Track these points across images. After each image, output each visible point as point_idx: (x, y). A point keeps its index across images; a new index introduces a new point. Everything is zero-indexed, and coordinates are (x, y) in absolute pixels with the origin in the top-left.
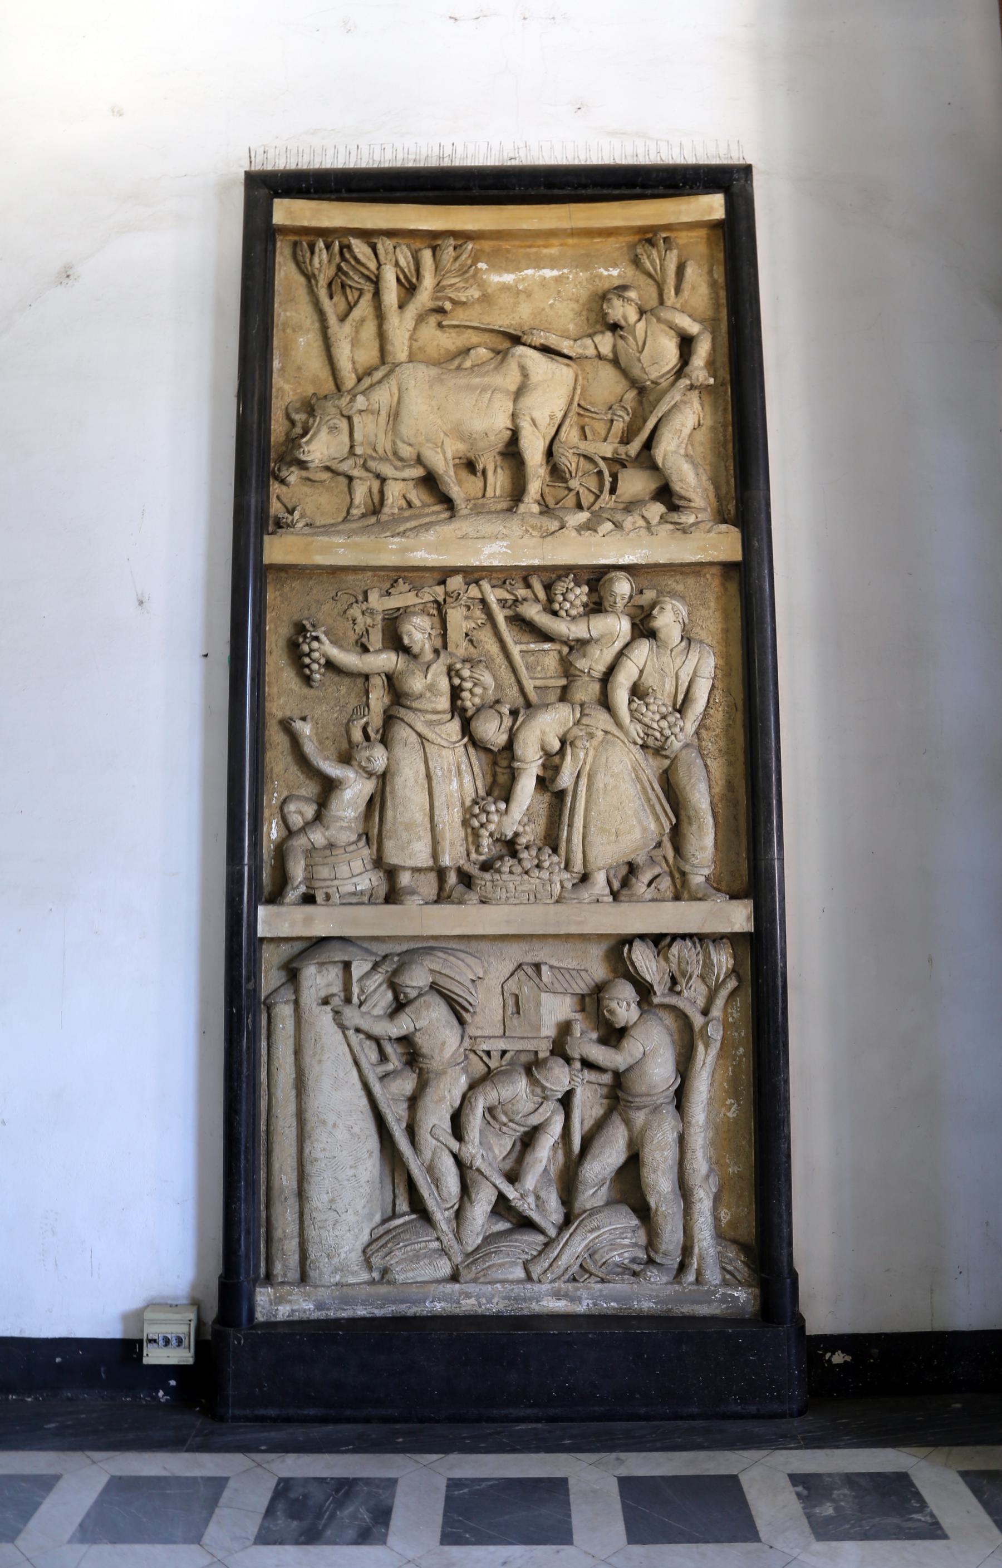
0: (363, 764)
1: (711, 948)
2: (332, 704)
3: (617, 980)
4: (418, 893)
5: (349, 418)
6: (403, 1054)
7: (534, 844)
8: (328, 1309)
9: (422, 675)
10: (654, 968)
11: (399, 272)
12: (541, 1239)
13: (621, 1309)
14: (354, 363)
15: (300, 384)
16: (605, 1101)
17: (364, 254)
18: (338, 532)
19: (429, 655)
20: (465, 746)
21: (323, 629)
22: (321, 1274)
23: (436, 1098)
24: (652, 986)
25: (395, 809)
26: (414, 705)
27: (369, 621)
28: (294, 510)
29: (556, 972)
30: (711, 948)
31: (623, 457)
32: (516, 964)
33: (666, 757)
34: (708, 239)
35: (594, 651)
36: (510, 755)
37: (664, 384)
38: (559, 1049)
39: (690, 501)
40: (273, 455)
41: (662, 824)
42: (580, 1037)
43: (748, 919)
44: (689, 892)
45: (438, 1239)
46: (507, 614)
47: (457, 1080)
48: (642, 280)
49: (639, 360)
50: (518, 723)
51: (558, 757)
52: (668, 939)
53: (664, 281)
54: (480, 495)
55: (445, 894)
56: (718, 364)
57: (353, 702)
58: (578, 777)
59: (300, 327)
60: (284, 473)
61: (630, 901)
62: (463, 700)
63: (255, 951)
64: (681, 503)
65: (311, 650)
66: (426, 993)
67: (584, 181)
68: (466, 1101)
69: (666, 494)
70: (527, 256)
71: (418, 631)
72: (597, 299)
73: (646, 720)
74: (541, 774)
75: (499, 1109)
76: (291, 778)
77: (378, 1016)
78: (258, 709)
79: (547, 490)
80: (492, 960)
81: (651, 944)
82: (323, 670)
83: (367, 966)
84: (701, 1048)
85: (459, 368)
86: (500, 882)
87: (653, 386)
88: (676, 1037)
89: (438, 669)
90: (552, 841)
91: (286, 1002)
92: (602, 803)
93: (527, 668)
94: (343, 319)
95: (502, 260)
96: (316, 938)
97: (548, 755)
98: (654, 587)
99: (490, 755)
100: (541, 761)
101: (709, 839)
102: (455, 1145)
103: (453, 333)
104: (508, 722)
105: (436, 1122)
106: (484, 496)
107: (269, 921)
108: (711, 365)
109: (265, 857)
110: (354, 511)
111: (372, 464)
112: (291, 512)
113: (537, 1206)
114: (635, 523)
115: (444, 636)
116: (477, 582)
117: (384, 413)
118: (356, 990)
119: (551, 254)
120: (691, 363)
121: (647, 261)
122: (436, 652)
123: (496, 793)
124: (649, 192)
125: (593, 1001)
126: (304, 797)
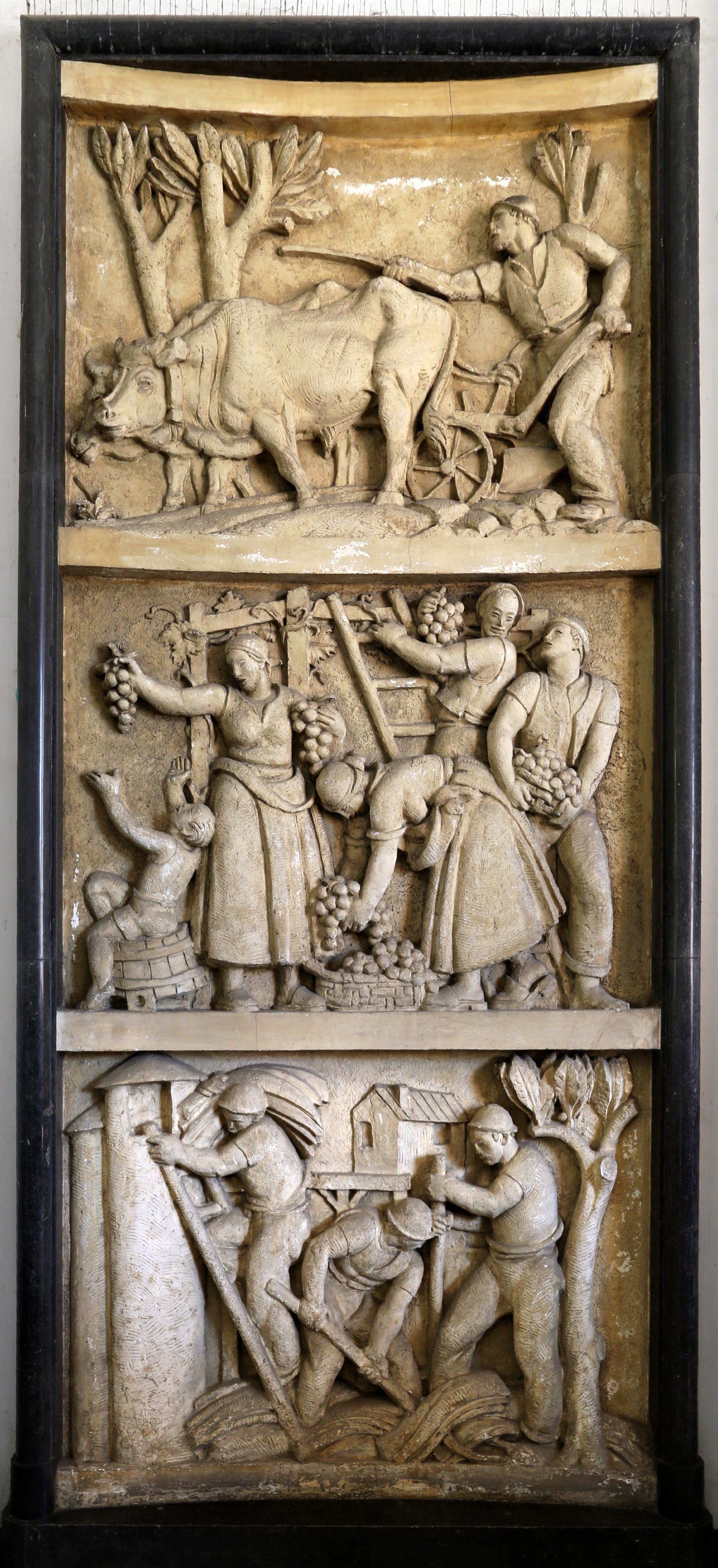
0: (185, 832)
1: (606, 1068)
2: (145, 755)
3: (491, 1106)
4: (251, 997)
5: (164, 371)
6: (232, 1194)
7: (393, 937)
8: (143, 1494)
9: (258, 717)
10: (537, 1093)
11: (226, 176)
12: (395, 1411)
13: (490, 1494)
14: (169, 301)
15: (101, 327)
16: (470, 1250)
17: (181, 147)
18: (152, 525)
19: (265, 692)
20: (310, 810)
21: (134, 654)
22: (134, 1452)
23: (272, 1248)
24: (532, 1114)
25: (224, 892)
26: (248, 756)
27: (191, 647)
28: (96, 496)
29: (417, 1096)
30: (606, 1068)
31: (511, 432)
32: (368, 1086)
33: (557, 827)
34: (631, 134)
35: (471, 688)
36: (365, 823)
37: (567, 332)
38: (420, 1188)
39: (596, 489)
40: (68, 422)
41: (550, 913)
42: (446, 1177)
43: (655, 1032)
44: (581, 999)
45: (273, 1411)
46: (363, 640)
47: (297, 1226)
48: (541, 191)
49: (536, 300)
50: (376, 781)
51: (424, 825)
52: (554, 1058)
53: (571, 192)
54: (329, 483)
55: (283, 999)
56: (636, 307)
57: (172, 753)
58: (449, 851)
59: (100, 248)
60: (82, 446)
61: (508, 1010)
62: (308, 750)
63: (53, 1069)
64: (586, 493)
65: (120, 682)
66: (261, 1121)
67: (473, 40)
68: (308, 1252)
69: (565, 481)
70: (391, 159)
71: (253, 659)
72: (481, 219)
73: (536, 779)
74: (402, 848)
75: (347, 1261)
76: (96, 850)
77: (203, 1149)
78: (54, 757)
79: (413, 476)
80: (339, 1080)
81: (533, 1063)
82: (134, 709)
83: (190, 1088)
84: (590, 1190)
85: (304, 308)
86: (353, 985)
87: (552, 335)
88: (558, 1176)
89: (277, 710)
90: (414, 932)
91: (92, 1131)
92: (479, 884)
93: (386, 711)
94: (155, 238)
95: (358, 165)
96: (128, 1052)
97: (410, 822)
98: (546, 606)
99: (339, 823)
100: (403, 831)
101: (607, 934)
102: (294, 1303)
103: (296, 263)
104: (363, 779)
105: (273, 1277)
106: (334, 484)
107: (71, 1031)
108: (627, 306)
109: (65, 950)
110: (172, 501)
111: (194, 436)
112: (92, 499)
113: (390, 1373)
114: (525, 519)
115: (284, 668)
116: (325, 598)
117: (208, 366)
118: (176, 1117)
119: (422, 157)
120: (604, 302)
121: (549, 164)
122: (275, 688)
123: (347, 872)
124: (558, 60)
125: (461, 1135)
126: (112, 874)
